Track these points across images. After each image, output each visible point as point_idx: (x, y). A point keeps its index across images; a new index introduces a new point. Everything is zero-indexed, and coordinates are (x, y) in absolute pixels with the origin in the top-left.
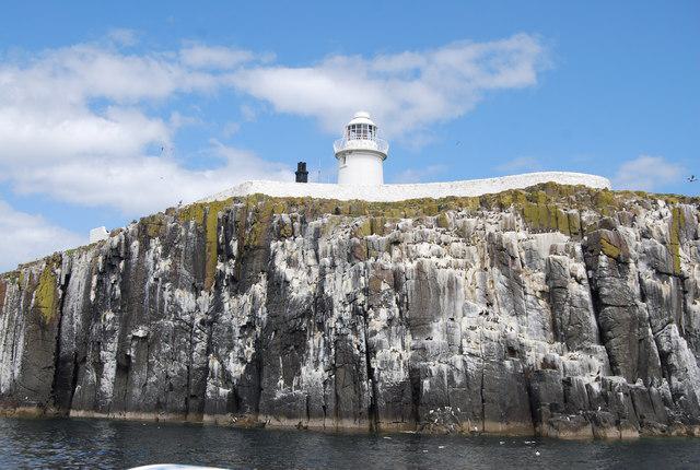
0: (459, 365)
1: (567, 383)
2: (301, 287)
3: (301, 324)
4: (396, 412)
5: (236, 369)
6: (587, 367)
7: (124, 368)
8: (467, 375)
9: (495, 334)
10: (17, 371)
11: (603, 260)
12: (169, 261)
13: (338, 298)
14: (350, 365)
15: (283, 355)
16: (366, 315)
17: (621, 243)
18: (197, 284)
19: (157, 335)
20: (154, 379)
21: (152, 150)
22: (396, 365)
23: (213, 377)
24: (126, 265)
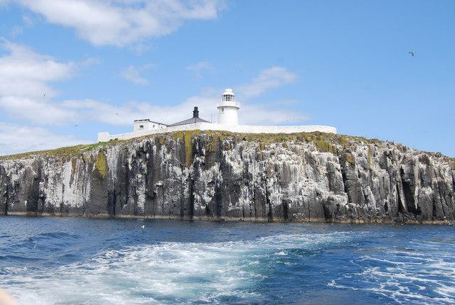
0: (301, 199)
1: (338, 205)
2: (237, 169)
4: (278, 215)
5: (208, 199)
6: (342, 199)
7: (151, 197)
8: (304, 203)
9: (313, 188)
10: (87, 199)
11: (347, 164)
12: (170, 155)
13: (254, 174)
14: (261, 198)
15: (231, 194)
16: (266, 181)
17: (353, 158)
20: (167, 202)
23: (197, 201)
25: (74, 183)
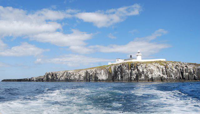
2: (141, 70)
4: (150, 80)
6: (165, 76)
7: (122, 77)
21: (58, 30)
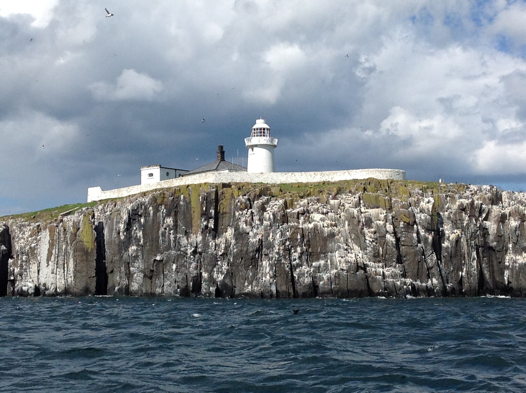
3: (255, 255)
18: (187, 231)
19: (169, 259)
22: (306, 275)
24: (146, 220)
25: (53, 259)
